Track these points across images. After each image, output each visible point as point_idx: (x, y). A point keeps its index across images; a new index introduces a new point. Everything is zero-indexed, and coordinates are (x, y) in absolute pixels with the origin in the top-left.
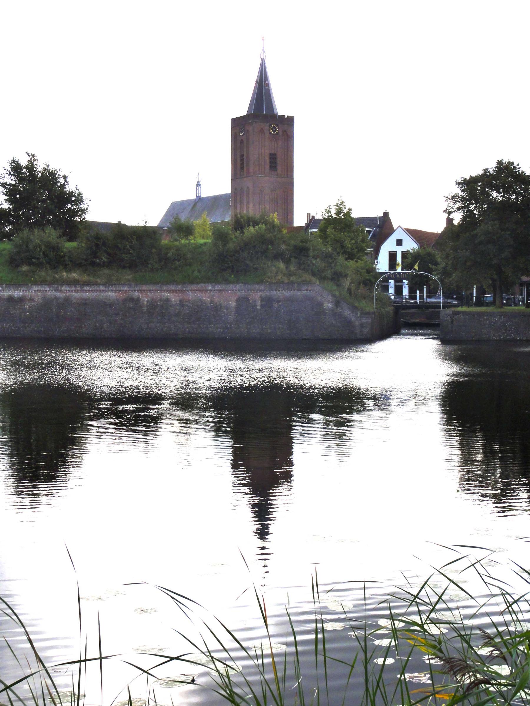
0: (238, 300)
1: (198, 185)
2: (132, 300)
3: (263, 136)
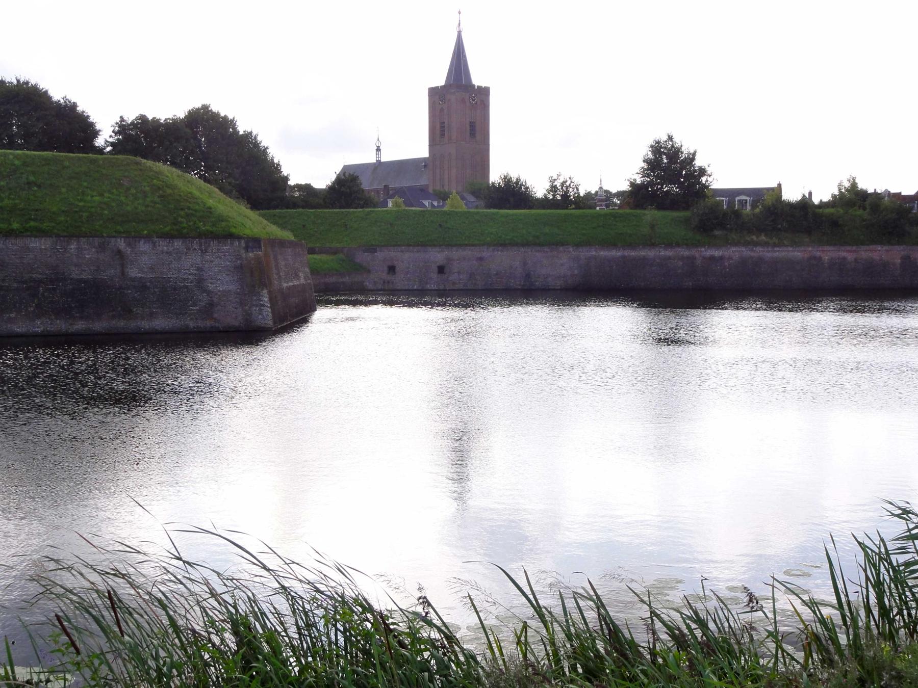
0: (902, 258)
1: (378, 149)
2: (815, 258)
3: (460, 108)
